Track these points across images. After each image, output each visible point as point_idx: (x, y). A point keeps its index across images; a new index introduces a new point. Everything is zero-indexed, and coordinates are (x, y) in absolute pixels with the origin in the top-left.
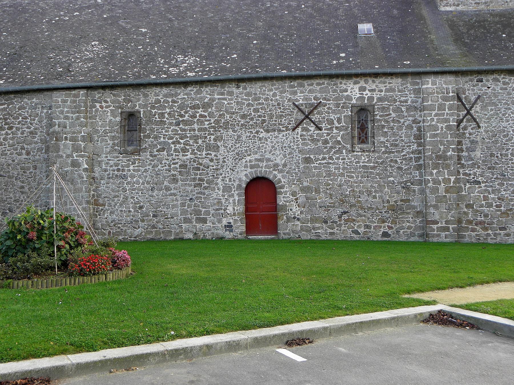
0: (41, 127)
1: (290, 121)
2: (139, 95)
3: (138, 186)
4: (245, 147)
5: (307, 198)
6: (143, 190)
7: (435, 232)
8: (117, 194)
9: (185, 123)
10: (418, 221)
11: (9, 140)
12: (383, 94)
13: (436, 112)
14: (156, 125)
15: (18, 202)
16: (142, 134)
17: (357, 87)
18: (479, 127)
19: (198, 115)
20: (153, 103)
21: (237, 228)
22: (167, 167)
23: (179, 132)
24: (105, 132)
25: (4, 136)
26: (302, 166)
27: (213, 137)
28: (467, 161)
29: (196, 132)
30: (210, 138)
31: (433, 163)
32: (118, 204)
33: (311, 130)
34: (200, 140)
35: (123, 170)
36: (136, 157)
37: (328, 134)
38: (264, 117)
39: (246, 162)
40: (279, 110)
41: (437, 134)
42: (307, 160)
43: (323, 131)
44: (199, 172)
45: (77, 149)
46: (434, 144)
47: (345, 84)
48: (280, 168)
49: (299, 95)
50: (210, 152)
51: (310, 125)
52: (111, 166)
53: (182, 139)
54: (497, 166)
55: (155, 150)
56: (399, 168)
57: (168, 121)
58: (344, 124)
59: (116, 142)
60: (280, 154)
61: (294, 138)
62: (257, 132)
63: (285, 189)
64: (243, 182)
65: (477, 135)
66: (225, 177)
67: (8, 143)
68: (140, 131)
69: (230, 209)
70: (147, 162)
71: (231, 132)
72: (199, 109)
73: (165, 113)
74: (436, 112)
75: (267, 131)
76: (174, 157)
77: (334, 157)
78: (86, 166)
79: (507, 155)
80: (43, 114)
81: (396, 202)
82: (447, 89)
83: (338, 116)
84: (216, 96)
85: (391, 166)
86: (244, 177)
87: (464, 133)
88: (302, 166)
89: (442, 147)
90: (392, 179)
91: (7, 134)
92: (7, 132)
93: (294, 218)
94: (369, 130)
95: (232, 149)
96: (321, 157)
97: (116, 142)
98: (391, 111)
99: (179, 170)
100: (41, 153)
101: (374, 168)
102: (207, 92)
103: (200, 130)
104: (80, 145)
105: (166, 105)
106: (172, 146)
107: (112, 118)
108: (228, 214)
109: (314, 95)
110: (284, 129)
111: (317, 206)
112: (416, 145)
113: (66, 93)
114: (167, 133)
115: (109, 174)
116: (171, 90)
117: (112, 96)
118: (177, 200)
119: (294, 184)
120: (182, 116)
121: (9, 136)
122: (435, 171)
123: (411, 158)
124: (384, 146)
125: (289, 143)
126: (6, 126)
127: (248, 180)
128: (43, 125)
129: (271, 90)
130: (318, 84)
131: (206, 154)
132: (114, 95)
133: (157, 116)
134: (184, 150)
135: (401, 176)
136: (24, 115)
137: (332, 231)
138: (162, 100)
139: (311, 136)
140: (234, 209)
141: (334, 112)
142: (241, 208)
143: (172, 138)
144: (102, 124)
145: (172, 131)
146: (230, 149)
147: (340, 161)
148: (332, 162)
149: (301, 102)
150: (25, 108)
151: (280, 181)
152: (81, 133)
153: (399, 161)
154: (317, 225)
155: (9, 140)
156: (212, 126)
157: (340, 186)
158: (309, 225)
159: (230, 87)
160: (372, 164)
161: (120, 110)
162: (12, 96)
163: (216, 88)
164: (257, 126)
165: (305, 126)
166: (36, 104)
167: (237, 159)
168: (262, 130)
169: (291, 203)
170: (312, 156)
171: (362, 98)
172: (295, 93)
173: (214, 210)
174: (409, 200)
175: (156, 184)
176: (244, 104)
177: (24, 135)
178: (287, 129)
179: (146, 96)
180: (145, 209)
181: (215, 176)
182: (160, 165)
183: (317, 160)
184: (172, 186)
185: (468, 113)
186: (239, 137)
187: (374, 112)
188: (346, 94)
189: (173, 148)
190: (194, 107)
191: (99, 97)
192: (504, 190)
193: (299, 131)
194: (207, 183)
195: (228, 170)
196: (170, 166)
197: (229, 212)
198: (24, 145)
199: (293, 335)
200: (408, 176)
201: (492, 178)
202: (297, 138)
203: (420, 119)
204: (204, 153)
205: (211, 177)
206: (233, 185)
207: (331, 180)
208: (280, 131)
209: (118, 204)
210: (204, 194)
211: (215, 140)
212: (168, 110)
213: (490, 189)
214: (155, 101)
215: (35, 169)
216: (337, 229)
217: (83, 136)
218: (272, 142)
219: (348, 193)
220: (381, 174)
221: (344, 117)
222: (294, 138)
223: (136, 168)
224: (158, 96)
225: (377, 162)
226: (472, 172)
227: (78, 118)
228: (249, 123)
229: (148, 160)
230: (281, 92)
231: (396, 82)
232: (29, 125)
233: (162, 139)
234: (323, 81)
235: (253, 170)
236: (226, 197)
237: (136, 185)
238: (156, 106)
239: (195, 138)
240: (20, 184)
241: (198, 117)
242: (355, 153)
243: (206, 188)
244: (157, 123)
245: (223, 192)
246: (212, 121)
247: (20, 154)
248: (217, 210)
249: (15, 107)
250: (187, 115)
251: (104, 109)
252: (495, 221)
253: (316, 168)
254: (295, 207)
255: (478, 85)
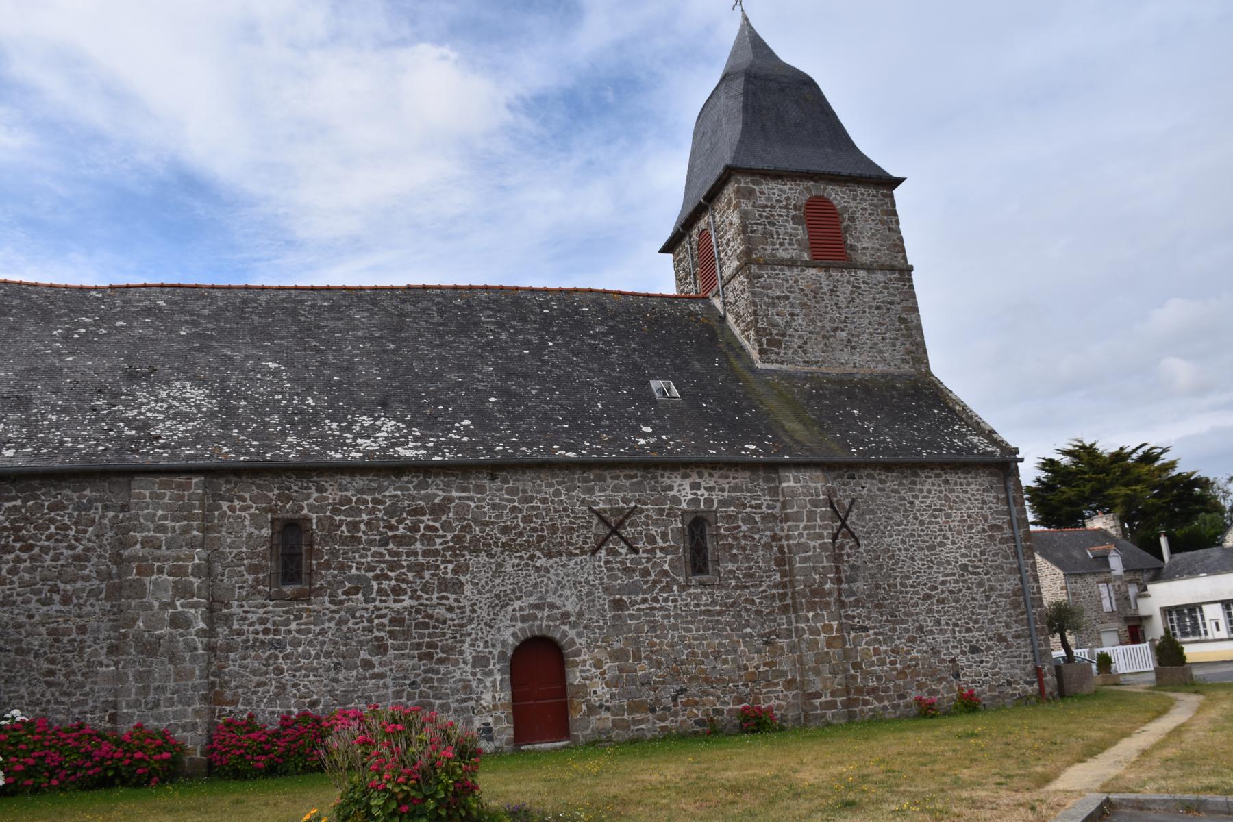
0: (100, 546)
1: (586, 538)
2: (308, 488)
3: (306, 661)
4: (511, 584)
5: (621, 670)
6: (316, 669)
7: (819, 712)
8: (263, 679)
9: (399, 540)
10: (790, 696)
11: (22, 573)
12: (726, 494)
13: (805, 523)
14: (343, 544)
15: (38, 704)
16: (314, 562)
17: (687, 484)
18: (859, 545)
19: (422, 526)
20: (336, 504)
21: (501, 732)
22: (366, 624)
23: (387, 557)
24: (239, 557)
25: (11, 564)
26: (609, 615)
27: (450, 567)
28: (847, 596)
29: (420, 558)
30: (446, 568)
31: (807, 602)
32: (265, 700)
33: (621, 554)
34: (426, 572)
35: (276, 632)
36: (301, 606)
37: (649, 560)
38: (542, 530)
39: (514, 610)
40: (567, 520)
41: (809, 556)
42: (618, 605)
43: (641, 554)
44: (426, 632)
45: (183, 591)
46: (807, 572)
47: (669, 478)
48: (572, 619)
49: (598, 494)
50: (445, 594)
51: (617, 544)
52: (251, 624)
53: (392, 571)
54: (886, 602)
55: (340, 592)
56: (758, 612)
57: (364, 537)
58: (672, 543)
59: (261, 576)
60: (572, 594)
61: (594, 567)
62: (532, 557)
63: (582, 657)
64: (509, 647)
65: (857, 557)
66: (476, 639)
67: (20, 578)
68: (311, 555)
69: (487, 698)
70: (324, 614)
71: (485, 557)
72: (425, 515)
73: (360, 522)
74: (805, 523)
75: (549, 555)
76: (377, 603)
77: (660, 598)
78: (202, 625)
79: (895, 586)
80: (106, 521)
81: (757, 667)
82: (816, 488)
83: (663, 528)
84: (455, 494)
85: (747, 610)
86: (511, 638)
87: (841, 555)
88: (609, 615)
89: (817, 577)
90: (748, 630)
91: (18, 560)
92: (18, 556)
93: (601, 706)
94: (709, 552)
95: (487, 588)
96: (639, 598)
97: (261, 576)
98: (740, 523)
99: (388, 628)
100: (98, 600)
101: (719, 613)
102: (437, 485)
103: (426, 553)
104: (191, 582)
105: (363, 507)
106: (374, 583)
107: (253, 530)
108: (484, 708)
109: (622, 494)
110: (578, 551)
111: (638, 683)
112: (778, 575)
113: (161, 482)
114: (362, 560)
115: (248, 641)
116: (370, 481)
117: (254, 488)
118: (385, 686)
119: (599, 647)
120: (391, 528)
121: (22, 566)
122: (811, 615)
123: (774, 595)
124: (735, 578)
125: (586, 575)
126: (18, 545)
127: (517, 644)
128: (105, 542)
129: (551, 485)
130: (628, 477)
131: (438, 598)
132: (259, 487)
133: (344, 528)
134: (397, 591)
135: (762, 625)
136: (60, 521)
137: (663, 724)
138: (354, 499)
139: (622, 563)
140: (494, 697)
141: (656, 523)
142: (505, 696)
143: (373, 569)
144: (233, 542)
145: (373, 556)
146: (483, 587)
147: (670, 604)
148: (658, 606)
149: (601, 505)
150: (65, 508)
151: (573, 642)
152: (194, 559)
153: (758, 601)
154: (638, 716)
155: (22, 573)
156: (449, 547)
157: (672, 645)
158: (626, 717)
159: (478, 478)
160: (718, 608)
161: (269, 516)
162: (36, 483)
163: (454, 479)
164: (529, 547)
165: (611, 546)
166: (90, 501)
167: (497, 605)
168: (538, 553)
169: (594, 680)
170: (625, 598)
171: (695, 501)
172: (590, 491)
173: (457, 701)
174: (776, 662)
175: (344, 658)
176: (504, 507)
177: (60, 563)
178: (583, 552)
179: (321, 489)
180: (321, 707)
181: (459, 638)
182: (352, 621)
183: (634, 603)
184: (375, 659)
185: (844, 525)
186: (500, 565)
187: (717, 523)
188: (670, 493)
189: (376, 588)
190: (417, 512)
191: (229, 490)
192: (898, 638)
193: (603, 555)
194: (443, 652)
195: (482, 625)
196: (370, 621)
197: (485, 704)
198: (59, 582)
199: (622, 754)
200: (772, 624)
201: (881, 621)
202: (600, 566)
203: (781, 534)
204: (435, 595)
205: (450, 641)
206: (490, 653)
207: (657, 637)
208: (570, 555)
209: (265, 700)
210: (438, 672)
211: (455, 572)
212: (365, 517)
213: (881, 638)
214: (341, 499)
215: (84, 633)
216: (672, 721)
217: (198, 566)
218: (557, 575)
219: (684, 657)
220: (733, 623)
221: (672, 530)
222: (594, 567)
223: (303, 627)
224: (346, 490)
225: (726, 605)
226: (855, 613)
227: (186, 530)
228: (514, 540)
229: (327, 612)
230: (569, 489)
231: (743, 478)
232: (73, 542)
233: (354, 571)
234: (635, 472)
235: (526, 625)
236: (479, 676)
237: (302, 661)
238: (343, 508)
239: (418, 568)
240: (45, 666)
241: (422, 531)
242: (692, 591)
243: (441, 661)
244: (344, 541)
245: (474, 666)
246: (449, 537)
247: (47, 602)
248: (464, 701)
249: (43, 505)
250: (401, 526)
251: (238, 512)
252: (891, 685)
253: (632, 617)
254: (600, 688)
255: (849, 483)
